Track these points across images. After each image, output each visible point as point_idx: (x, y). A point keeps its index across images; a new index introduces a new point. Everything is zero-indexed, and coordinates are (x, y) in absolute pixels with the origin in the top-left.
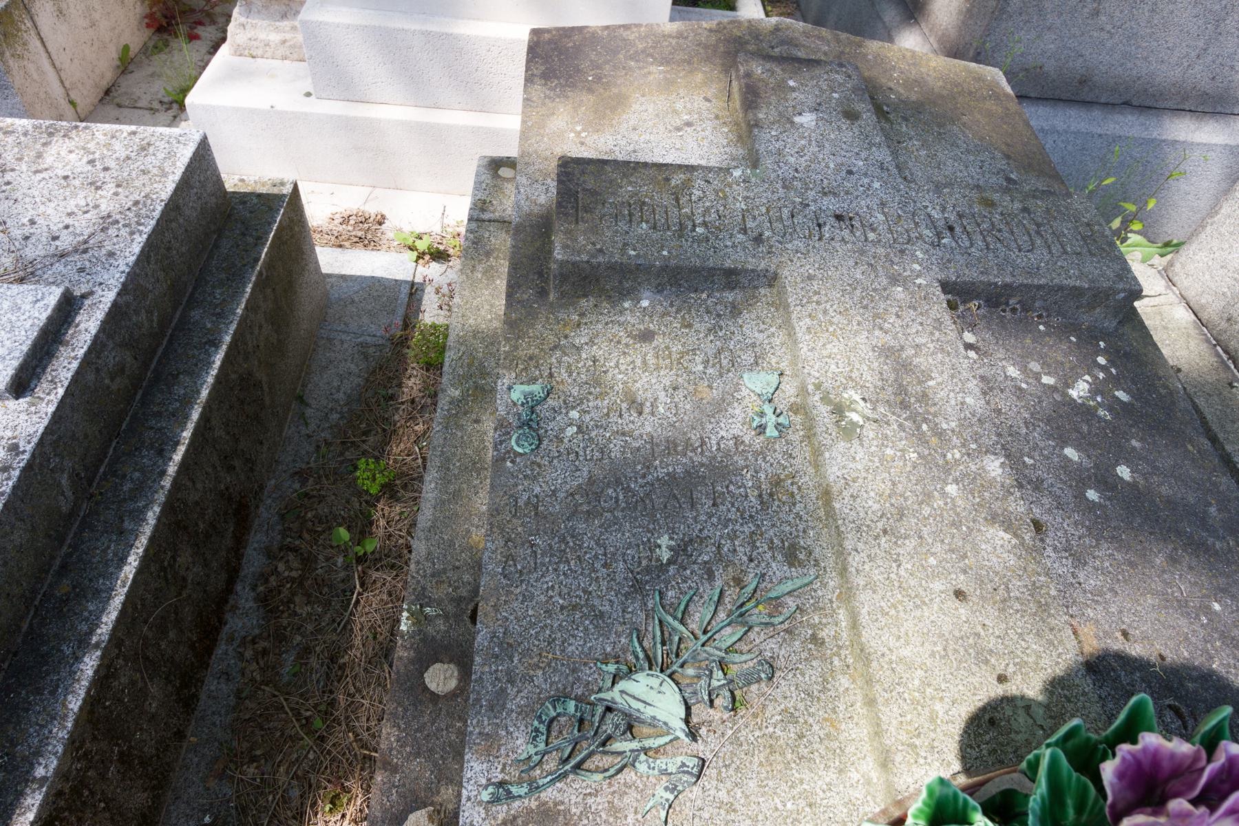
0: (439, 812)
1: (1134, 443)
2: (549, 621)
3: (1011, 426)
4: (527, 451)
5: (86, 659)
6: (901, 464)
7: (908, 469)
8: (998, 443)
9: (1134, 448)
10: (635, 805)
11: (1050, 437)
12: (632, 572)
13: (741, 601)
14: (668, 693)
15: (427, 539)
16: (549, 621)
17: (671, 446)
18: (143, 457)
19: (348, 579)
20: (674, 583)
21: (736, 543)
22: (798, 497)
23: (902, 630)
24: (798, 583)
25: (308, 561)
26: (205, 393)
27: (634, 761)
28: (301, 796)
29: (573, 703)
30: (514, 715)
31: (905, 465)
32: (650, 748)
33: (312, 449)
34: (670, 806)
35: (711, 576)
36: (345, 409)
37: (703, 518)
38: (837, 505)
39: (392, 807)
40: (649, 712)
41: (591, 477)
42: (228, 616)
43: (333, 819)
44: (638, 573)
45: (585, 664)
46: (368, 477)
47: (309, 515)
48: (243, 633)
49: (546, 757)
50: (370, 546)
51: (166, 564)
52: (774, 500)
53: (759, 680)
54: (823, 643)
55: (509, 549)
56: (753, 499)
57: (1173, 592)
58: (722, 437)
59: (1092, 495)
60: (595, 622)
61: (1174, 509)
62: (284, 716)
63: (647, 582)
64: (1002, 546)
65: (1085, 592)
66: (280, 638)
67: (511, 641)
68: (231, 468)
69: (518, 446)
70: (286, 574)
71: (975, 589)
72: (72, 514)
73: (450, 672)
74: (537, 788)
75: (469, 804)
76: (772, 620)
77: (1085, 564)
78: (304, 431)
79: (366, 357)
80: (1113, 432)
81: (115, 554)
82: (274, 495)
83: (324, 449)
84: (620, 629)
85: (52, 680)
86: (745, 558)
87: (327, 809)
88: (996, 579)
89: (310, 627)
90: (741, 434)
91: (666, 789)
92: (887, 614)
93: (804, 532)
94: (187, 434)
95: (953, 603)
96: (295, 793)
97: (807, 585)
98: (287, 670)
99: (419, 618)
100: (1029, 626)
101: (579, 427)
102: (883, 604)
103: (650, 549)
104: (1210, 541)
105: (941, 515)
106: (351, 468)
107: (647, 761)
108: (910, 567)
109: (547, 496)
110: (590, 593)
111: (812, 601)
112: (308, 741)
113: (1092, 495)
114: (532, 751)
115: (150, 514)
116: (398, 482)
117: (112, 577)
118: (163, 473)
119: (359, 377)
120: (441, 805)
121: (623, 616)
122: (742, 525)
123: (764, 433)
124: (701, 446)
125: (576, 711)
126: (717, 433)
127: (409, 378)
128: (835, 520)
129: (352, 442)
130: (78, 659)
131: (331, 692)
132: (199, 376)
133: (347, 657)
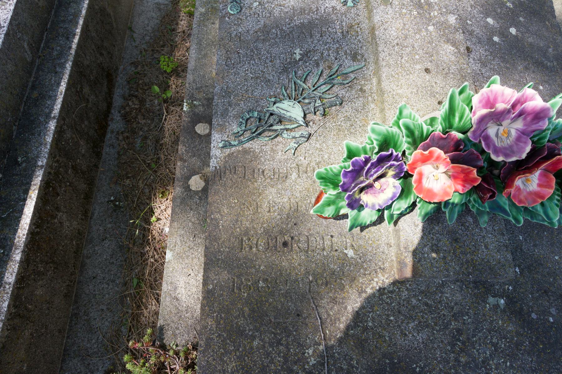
0: (204, 176)
1: (521, 19)
2: (246, 83)
3: (464, 7)
4: (235, 13)
5: (51, 123)
6: (409, 16)
7: (412, 19)
8: (456, 9)
9: (520, 21)
10: (281, 149)
11: (482, 13)
12: (283, 64)
13: (330, 74)
14: (296, 108)
15: (193, 74)
16: (246, 83)
17: (302, 11)
18: (60, 40)
19: (160, 110)
20: (301, 68)
21: (330, 52)
22: (360, 33)
23: (400, 83)
24: (356, 68)
25: (142, 102)
26: (84, 12)
27: (282, 133)
28: (149, 192)
29: (256, 113)
30: (232, 118)
31: (411, 17)
32: (289, 128)
33: (138, 53)
34: (296, 149)
35: (318, 65)
36: (152, 35)
37: (316, 42)
38: (377, 33)
39: (185, 174)
40: (288, 114)
41: (265, 25)
42: (110, 123)
43: (163, 200)
44: (285, 64)
45: (262, 99)
46: (165, 65)
47: (140, 82)
48: (117, 130)
49: (245, 133)
50: (169, 94)
51: (78, 90)
52: (348, 34)
53: (336, 105)
54: (365, 91)
55: (228, 55)
56: (339, 34)
57: (523, 81)
58: (327, 7)
59: (496, 39)
60: (266, 83)
61: (532, 48)
62: (139, 162)
63: (289, 68)
64: (450, 52)
65: (484, 77)
66: (133, 132)
67: (230, 91)
68: (101, 54)
69: (231, 10)
70: (133, 106)
71: (435, 69)
72: (32, 63)
73: (206, 127)
74: (242, 142)
75: (214, 148)
76: (344, 82)
77: (487, 66)
78: (134, 44)
79: (160, 10)
80: (512, 13)
81: (55, 82)
82: (123, 73)
83: (144, 53)
84: (277, 86)
85: (38, 130)
86: (333, 58)
87: (160, 196)
88: (445, 65)
89: (146, 129)
90: (336, 5)
91: (295, 143)
92: (394, 77)
93: (361, 47)
94: (78, 31)
95: (424, 74)
96: (147, 191)
97: (360, 69)
98: (138, 145)
99: (191, 106)
100: (456, 84)
101: (260, 3)
102: (392, 73)
103: (291, 55)
104: (545, 62)
105: (424, 39)
106: (157, 62)
107: (287, 133)
108: (407, 59)
109: (245, 33)
110: (264, 72)
111: (361, 75)
112: (150, 172)
113: (496, 39)
114: (239, 129)
115: (67, 65)
116: (179, 69)
117: (56, 91)
118: (70, 48)
119: (157, 19)
120: (205, 174)
121: (278, 81)
122: (333, 44)
123: (347, 5)
124: (317, 11)
125: (258, 115)
126: (325, 5)
127: (181, 20)
128: (375, 40)
129: (156, 50)
130: (47, 123)
131: (158, 154)
132: (80, 4)
133: (163, 141)
